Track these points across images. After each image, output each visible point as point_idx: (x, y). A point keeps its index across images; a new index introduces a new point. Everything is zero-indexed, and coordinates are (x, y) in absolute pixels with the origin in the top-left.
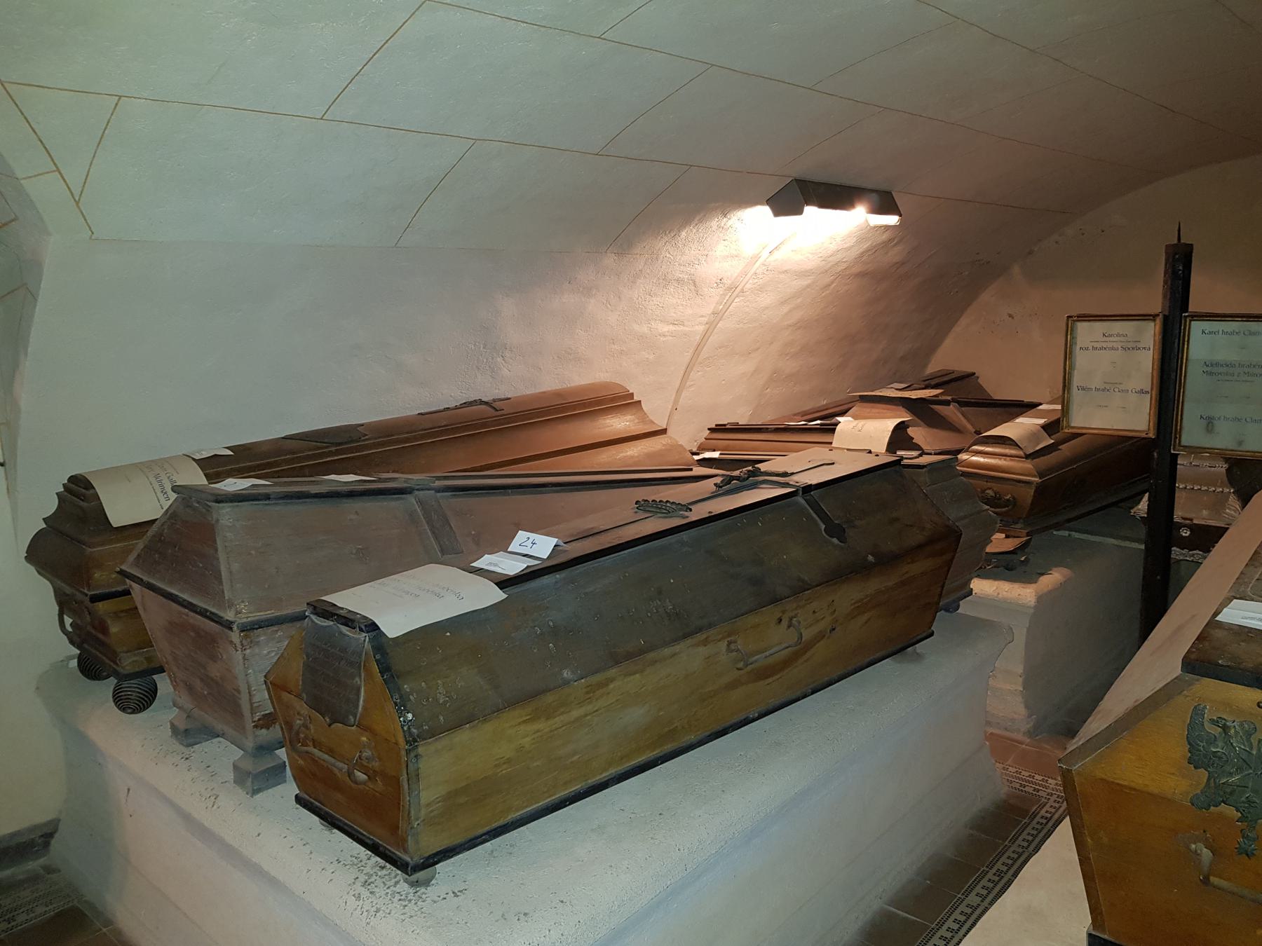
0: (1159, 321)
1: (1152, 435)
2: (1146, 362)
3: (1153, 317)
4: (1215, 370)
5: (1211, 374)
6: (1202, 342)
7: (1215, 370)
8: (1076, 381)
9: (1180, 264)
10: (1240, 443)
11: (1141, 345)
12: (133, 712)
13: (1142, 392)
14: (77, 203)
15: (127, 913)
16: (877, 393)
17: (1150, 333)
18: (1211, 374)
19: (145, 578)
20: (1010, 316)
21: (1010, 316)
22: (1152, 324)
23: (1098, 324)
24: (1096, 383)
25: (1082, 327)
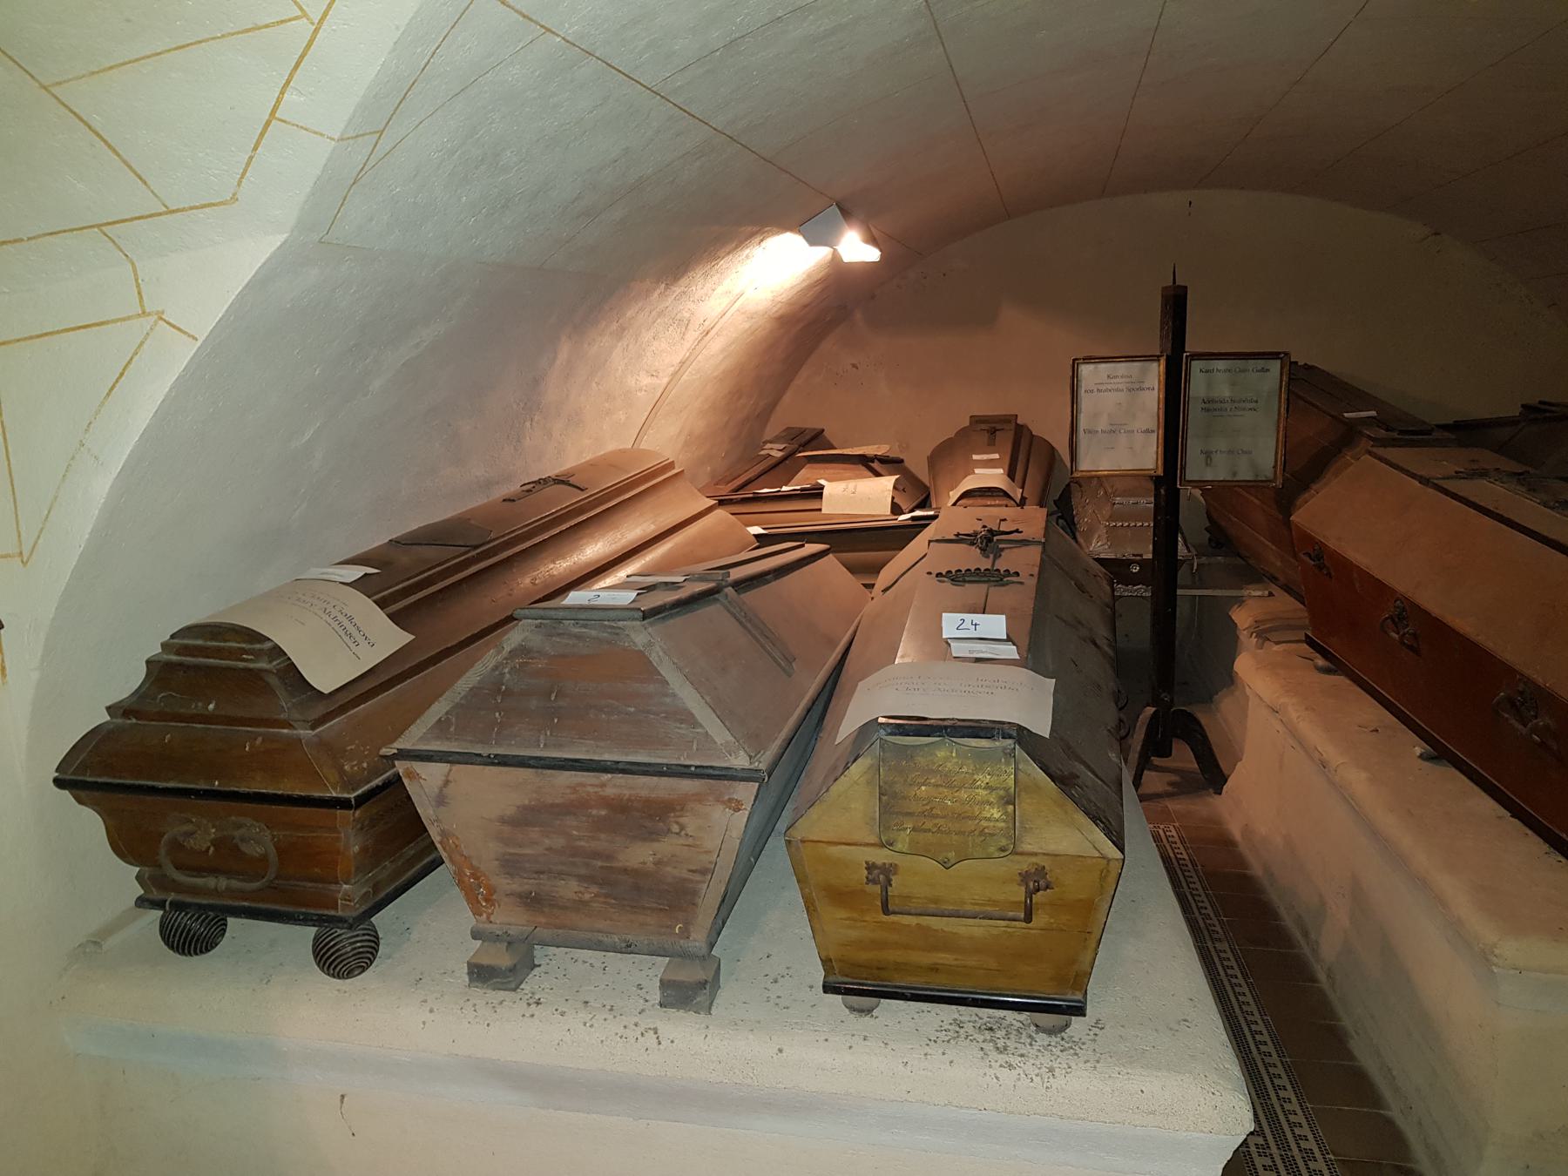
0: (1163, 361)
1: (1160, 472)
2: (1152, 399)
3: (1156, 358)
4: (1211, 406)
5: (1208, 410)
6: (1201, 381)
7: (1211, 406)
8: (1083, 423)
9: (1176, 304)
10: (1235, 474)
11: (1146, 385)
12: (364, 969)
13: (1147, 431)
14: (99, 226)
15: (1423, 1163)
16: (846, 452)
17: (1154, 374)
18: (1208, 410)
19: (485, 752)
20: (854, 366)
21: (854, 366)
22: (1155, 365)
24: (1103, 424)
25: (1086, 370)
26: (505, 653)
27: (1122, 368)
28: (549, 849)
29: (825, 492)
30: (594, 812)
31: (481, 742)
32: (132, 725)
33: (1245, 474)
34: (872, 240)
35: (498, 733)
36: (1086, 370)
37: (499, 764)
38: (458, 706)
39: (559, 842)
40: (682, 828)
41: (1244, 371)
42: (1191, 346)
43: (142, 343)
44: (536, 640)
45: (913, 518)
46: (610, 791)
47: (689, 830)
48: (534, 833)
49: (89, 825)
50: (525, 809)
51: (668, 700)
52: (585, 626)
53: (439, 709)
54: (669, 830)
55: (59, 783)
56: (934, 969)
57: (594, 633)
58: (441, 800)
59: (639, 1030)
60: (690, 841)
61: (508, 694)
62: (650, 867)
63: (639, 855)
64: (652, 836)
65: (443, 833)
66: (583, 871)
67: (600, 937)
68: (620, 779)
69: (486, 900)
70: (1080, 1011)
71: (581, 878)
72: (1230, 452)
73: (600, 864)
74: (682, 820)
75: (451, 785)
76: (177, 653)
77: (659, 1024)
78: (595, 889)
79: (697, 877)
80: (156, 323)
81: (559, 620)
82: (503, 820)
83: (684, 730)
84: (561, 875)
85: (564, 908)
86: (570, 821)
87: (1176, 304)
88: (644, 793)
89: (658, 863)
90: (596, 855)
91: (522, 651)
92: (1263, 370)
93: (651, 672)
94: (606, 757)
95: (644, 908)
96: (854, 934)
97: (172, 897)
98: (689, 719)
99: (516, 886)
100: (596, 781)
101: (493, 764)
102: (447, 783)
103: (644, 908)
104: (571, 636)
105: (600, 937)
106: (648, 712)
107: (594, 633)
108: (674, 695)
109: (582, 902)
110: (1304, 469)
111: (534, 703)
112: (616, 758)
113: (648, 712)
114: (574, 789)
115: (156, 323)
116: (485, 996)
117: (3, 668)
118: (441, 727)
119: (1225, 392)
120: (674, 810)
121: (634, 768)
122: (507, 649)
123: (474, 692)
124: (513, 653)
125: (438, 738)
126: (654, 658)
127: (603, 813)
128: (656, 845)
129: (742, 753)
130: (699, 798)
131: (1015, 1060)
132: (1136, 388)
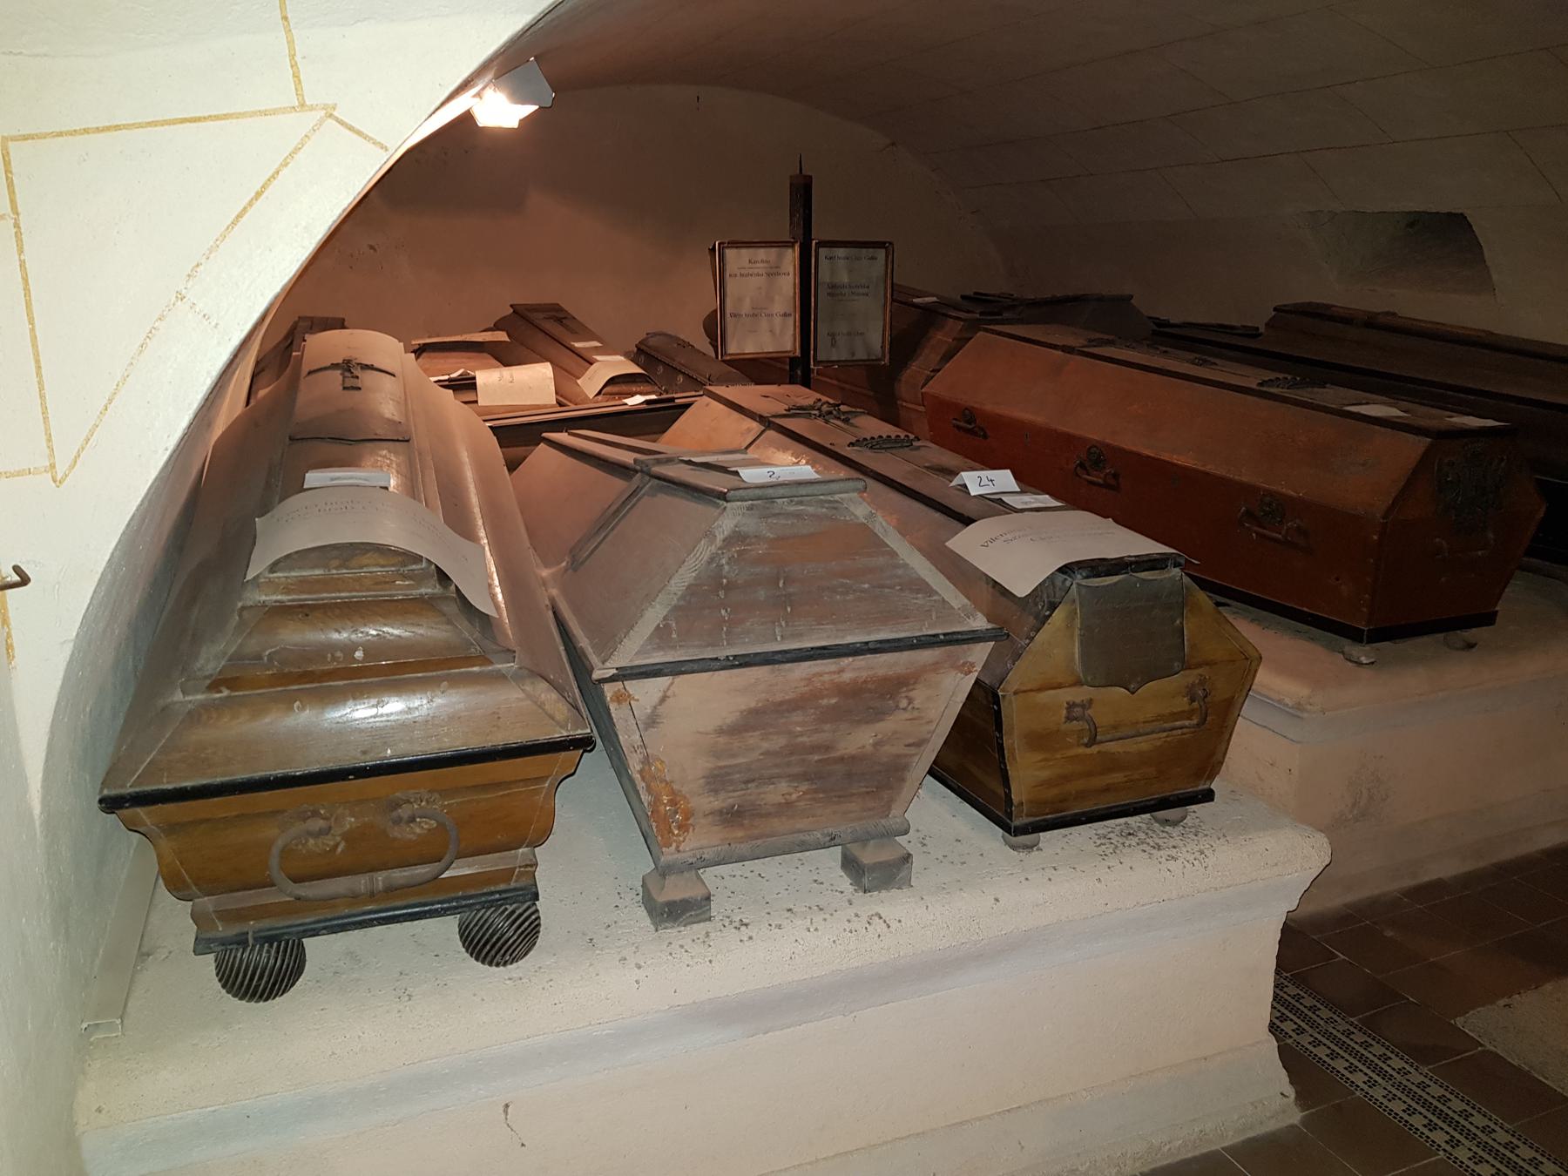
0: (797, 248)
2: (788, 283)
6: (834, 267)
9: (802, 192)
13: (785, 315)
17: (791, 257)
20: (372, 247)
21: (372, 247)
23: (744, 251)
24: (746, 308)
26: (719, 542)
27: (762, 253)
28: (767, 753)
29: (479, 381)
30: (825, 702)
31: (713, 645)
32: (228, 697)
33: (861, 355)
34: (519, 97)
35: (728, 633)
36: (730, 253)
37: (740, 666)
38: (676, 608)
39: (778, 742)
40: (910, 701)
41: (858, 259)
42: (817, 234)
43: (296, 150)
44: (750, 524)
45: (647, 402)
46: (847, 676)
47: (917, 704)
48: (753, 738)
49: (131, 853)
50: (754, 712)
51: (900, 572)
52: (801, 503)
53: (654, 615)
54: (897, 707)
55: (111, 804)
56: (1107, 789)
57: (811, 509)
58: (652, 721)
59: (864, 918)
60: (916, 714)
61: (729, 588)
62: (869, 749)
63: (860, 739)
64: (879, 715)
65: (646, 761)
66: (796, 770)
67: (801, 837)
68: (860, 661)
69: (679, 828)
70: (1208, 796)
71: (793, 778)
72: (849, 334)
73: (816, 758)
74: (911, 694)
75: (669, 701)
76: (287, 591)
77: (880, 910)
78: (804, 787)
79: (912, 750)
80: (321, 122)
81: (772, 499)
82: (721, 731)
83: (920, 600)
84: (771, 780)
85: (769, 815)
86: (797, 717)
87: (802, 192)
88: (881, 672)
89: (875, 745)
90: (815, 748)
91: (736, 537)
92: (873, 258)
93: (879, 545)
94: (849, 639)
95: (853, 795)
96: (1045, 774)
97: (252, 925)
98: (923, 588)
99: (717, 803)
100: (833, 668)
101: (733, 667)
102: (663, 699)
103: (853, 795)
104: (788, 515)
105: (801, 837)
106: (882, 586)
107: (811, 509)
108: (906, 566)
109: (789, 804)
110: (904, 344)
111: (762, 594)
112: (866, 639)
113: (882, 586)
114: (809, 680)
115: (321, 122)
116: (671, 932)
117: (9, 647)
118: (661, 635)
119: (844, 278)
120: (907, 685)
121: (695, 666)
122: (720, 537)
123: (691, 590)
124: (729, 541)
125: (660, 648)
126: (878, 530)
127: (834, 701)
128: (880, 726)
129: (979, 615)
130: (935, 667)
131: (1173, 852)
132: (774, 272)
